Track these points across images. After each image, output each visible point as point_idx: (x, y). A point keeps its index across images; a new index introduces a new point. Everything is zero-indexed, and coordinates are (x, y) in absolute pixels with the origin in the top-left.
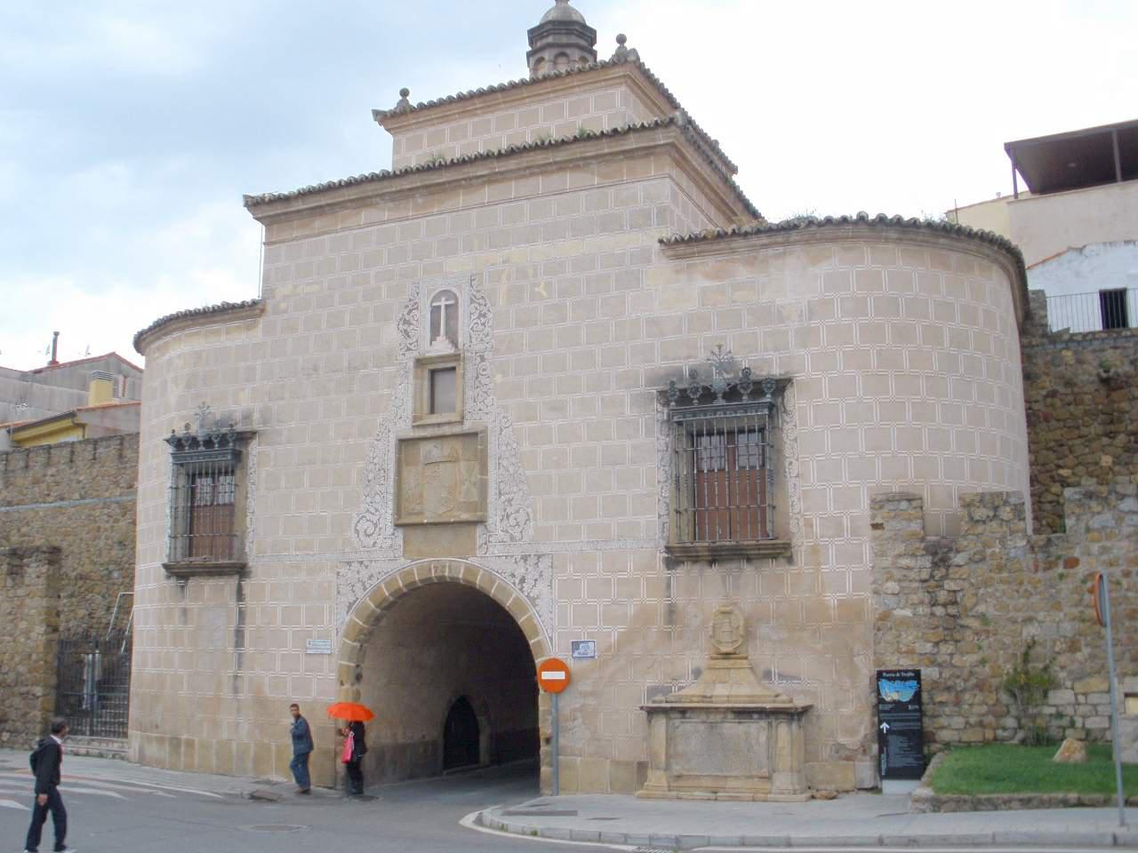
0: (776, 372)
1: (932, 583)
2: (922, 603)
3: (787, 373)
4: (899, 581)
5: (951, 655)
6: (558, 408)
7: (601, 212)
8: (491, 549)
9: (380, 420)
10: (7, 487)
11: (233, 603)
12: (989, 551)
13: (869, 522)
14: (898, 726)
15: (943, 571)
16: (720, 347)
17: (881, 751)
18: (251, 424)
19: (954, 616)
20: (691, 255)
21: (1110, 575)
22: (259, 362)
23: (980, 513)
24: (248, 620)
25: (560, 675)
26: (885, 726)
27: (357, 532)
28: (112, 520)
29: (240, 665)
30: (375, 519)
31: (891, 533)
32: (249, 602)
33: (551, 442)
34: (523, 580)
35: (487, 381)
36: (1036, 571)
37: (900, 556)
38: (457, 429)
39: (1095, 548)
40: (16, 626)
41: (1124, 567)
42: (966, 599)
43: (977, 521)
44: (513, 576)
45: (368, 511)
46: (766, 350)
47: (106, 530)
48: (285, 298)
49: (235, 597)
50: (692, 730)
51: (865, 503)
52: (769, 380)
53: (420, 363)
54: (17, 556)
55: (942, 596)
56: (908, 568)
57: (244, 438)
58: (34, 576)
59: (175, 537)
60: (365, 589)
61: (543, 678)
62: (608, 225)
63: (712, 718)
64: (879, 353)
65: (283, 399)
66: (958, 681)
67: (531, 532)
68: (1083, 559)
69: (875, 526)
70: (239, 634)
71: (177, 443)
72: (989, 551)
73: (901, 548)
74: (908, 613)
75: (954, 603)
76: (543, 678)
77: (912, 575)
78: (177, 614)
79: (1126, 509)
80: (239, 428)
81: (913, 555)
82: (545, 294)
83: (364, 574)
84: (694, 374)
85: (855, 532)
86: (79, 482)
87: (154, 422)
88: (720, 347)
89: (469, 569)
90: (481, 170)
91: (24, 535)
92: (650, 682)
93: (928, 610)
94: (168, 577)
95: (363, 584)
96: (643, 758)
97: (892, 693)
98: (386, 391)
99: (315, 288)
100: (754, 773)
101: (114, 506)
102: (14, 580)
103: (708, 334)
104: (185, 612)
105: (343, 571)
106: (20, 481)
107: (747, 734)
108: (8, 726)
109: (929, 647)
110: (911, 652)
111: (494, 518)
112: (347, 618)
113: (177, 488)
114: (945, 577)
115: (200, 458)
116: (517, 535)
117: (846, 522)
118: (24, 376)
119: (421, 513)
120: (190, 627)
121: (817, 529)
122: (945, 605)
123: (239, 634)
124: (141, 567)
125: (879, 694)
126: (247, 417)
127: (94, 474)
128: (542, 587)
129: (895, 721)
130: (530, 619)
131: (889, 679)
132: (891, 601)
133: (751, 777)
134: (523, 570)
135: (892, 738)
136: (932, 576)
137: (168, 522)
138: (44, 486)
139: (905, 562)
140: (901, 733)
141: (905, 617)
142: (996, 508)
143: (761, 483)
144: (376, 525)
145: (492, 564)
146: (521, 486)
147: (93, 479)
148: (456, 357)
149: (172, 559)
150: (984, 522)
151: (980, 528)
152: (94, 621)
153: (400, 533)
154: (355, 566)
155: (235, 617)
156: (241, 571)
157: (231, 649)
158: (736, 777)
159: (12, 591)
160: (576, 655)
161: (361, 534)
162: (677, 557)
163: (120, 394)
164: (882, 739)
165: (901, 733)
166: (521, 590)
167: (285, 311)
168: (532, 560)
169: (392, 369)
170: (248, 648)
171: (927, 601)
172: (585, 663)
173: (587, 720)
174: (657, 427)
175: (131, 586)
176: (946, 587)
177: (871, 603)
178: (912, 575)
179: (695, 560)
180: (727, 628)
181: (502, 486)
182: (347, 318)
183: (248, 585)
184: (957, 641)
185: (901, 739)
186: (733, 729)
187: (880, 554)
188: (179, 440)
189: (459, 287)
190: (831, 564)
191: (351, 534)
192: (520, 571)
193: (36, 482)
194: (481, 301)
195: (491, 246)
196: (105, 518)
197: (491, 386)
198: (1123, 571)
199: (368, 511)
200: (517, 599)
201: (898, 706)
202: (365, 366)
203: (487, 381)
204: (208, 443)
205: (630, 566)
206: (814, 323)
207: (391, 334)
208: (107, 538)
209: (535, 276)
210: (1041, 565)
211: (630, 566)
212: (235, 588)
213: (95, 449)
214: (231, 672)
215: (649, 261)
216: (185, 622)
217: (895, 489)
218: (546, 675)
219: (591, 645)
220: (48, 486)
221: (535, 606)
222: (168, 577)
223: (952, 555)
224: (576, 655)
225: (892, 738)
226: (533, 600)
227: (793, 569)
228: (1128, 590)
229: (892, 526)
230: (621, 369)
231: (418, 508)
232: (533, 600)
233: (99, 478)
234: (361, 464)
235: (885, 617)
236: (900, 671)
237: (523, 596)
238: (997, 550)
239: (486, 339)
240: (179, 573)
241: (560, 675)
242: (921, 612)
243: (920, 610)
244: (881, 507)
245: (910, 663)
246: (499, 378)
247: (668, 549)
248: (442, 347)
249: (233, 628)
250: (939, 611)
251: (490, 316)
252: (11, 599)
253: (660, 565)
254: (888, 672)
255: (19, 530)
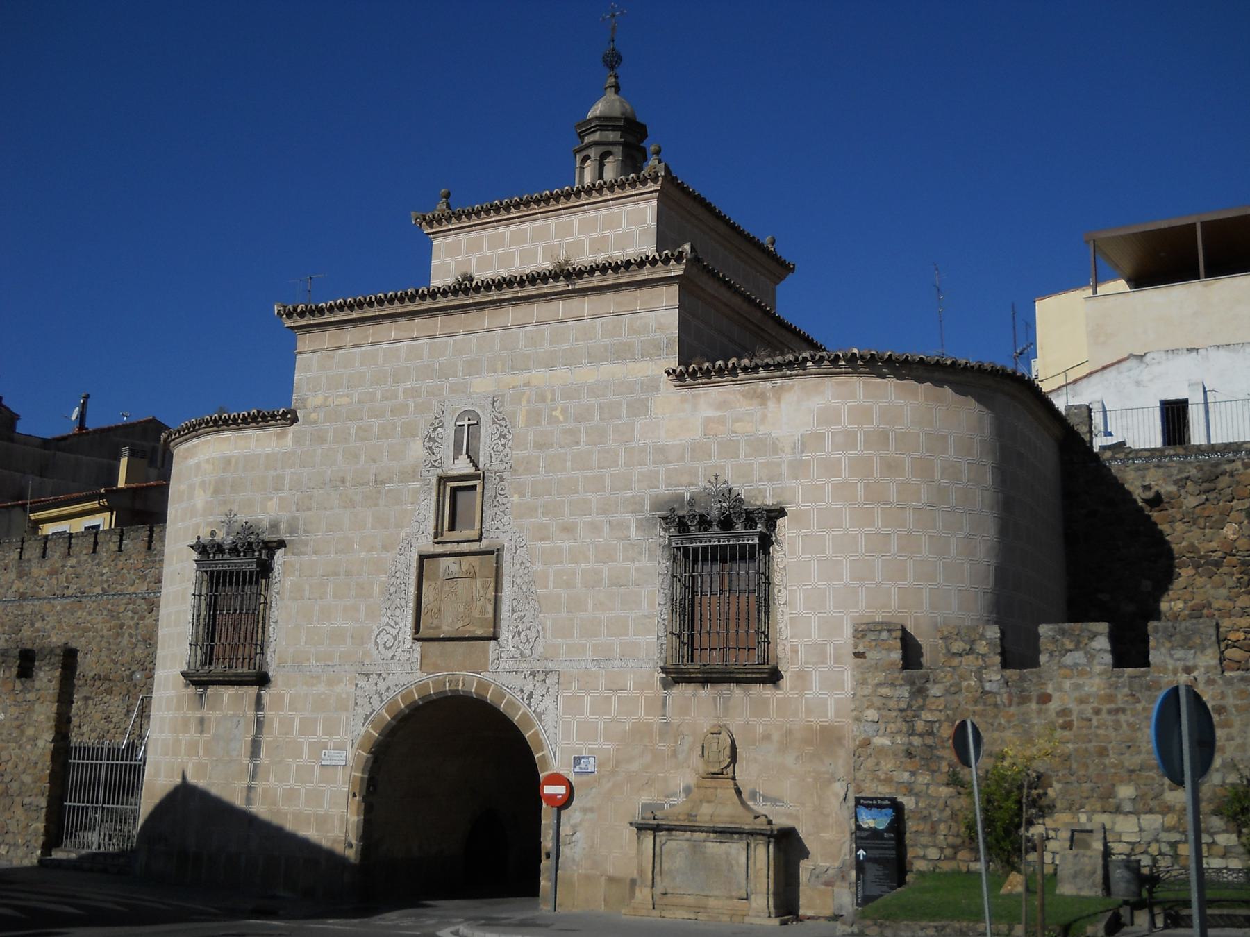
0: (770, 501)
1: (909, 713)
2: (899, 732)
3: (779, 503)
4: (879, 709)
5: (928, 785)
6: (568, 529)
7: (616, 340)
8: (502, 665)
9: (403, 534)
10: (21, 577)
11: (251, 714)
12: (965, 684)
13: (851, 650)
14: (876, 853)
15: (920, 701)
16: (716, 477)
17: (858, 878)
18: (278, 532)
19: (930, 746)
21: (1081, 712)
22: (288, 471)
23: (958, 646)
24: (265, 730)
26: (861, 852)
27: (377, 644)
28: (136, 617)
29: (254, 777)
30: (394, 632)
31: (873, 662)
32: (268, 713)
33: (561, 562)
34: (531, 696)
35: (505, 501)
36: (1010, 705)
37: (880, 685)
38: (475, 547)
39: (1067, 684)
40: (23, 733)
41: (1095, 705)
42: (942, 731)
43: (955, 654)
44: (522, 691)
45: (388, 624)
46: (761, 480)
47: (129, 627)
48: (316, 408)
49: (253, 707)
50: (676, 845)
51: (848, 632)
52: (760, 510)
53: (442, 480)
54: (26, 663)
55: (920, 726)
56: (887, 697)
57: (272, 547)
58: (45, 680)
59: (196, 645)
60: (382, 701)
61: (545, 792)
62: (623, 353)
63: (697, 835)
64: (867, 486)
65: (309, 509)
66: (933, 811)
67: (541, 649)
68: (1056, 695)
69: (858, 655)
71: (202, 549)
72: (965, 684)
73: (880, 677)
74: (886, 741)
75: (931, 733)
76: (545, 792)
77: (892, 704)
78: (193, 723)
79: (1098, 647)
80: (266, 537)
81: (893, 685)
82: (561, 418)
83: (382, 686)
84: (692, 502)
85: (837, 659)
86: (102, 575)
88: (716, 477)
89: (480, 684)
90: (506, 294)
91: (38, 630)
92: (645, 799)
93: (906, 740)
94: (187, 686)
95: (381, 696)
96: (635, 875)
97: (870, 820)
98: (410, 507)
99: (345, 400)
100: (734, 894)
101: (139, 601)
102: (23, 684)
103: (710, 463)
104: (202, 721)
105: (361, 683)
106: (35, 571)
107: (728, 854)
108: (8, 838)
109: (906, 776)
110: (888, 781)
111: (505, 633)
112: (363, 730)
113: (200, 595)
114: (922, 708)
115: (223, 563)
116: (527, 652)
117: (830, 650)
118: (46, 443)
119: (438, 627)
120: (207, 736)
121: (802, 654)
122: (921, 735)
124: (159, 674)
125: (857, 820)
126: (274, 526)
127: (119, 567)
128: (548, 701)
129: (871, 848)
130: (536, 734)
131: (867, 806)
132: (871, 729)
133: (731, 898)
134: (531, 686)
135: (868, 866)
136: (910, 706)
137: (188, 630)
138: (62, 578)
139: (884, 691)
140: (875, 861)
141: (883, 746)
142: (973, 642)
143: (255, 625)
144: (395, 638)
145: (502, 677)
146: (532, 603)
147: (118, 572)
148: (475, 477)
149: (192, 667)
150: (961, 655)
151: (956, 662)
152: (112, 726)
153: (418, 645)
154: (373, 678)
156: (262, 680)
157: (246, 760)
158: (716, 897)
159: (21, 695)
160: (577, 769)
162: (675, 676)
163: (159, 464)
164: (860, 866)
165: (875, 861)
166: (529, 705)
167: (315, 422)
168: (540, 677)
169: (416, 485)
170: (264, 759)
171: (904, 730)
172: (585, 778)
173: (589, 844)
174: (659, 551)
175: (150, 690)
176: (923, 717)
177: (853, 733)
178: (892, 704)
179: (689, 680)
180: (715, 747)
181: (515, 603)
182: (376, 431)
183: (267, 694)
184: (933, 772)
185: (877, 866)
186: (715, 848)
188: (204, 546)
189: (482, 407)
190: (815, 690)
191: (371, 646)
192: (528, 687)
193: (54, 573)
194: (502, 422)
195: (513, 369)
196: (130, 614)
197: (509, 505)
198: (1093, 708)
199: (388, 624)
200: (525, 714)
201: (874, 833)
203: (505, 501)
204: (234, 550)
205: (630, 684)
207: (417, 450)
208: (131, 635)
209: (553, 400)
210: (1015, 700)
211: (630, 684)
212: (254, 697)
213: (121, 541)
214: (244, 783)
215: (657, 389)
216: (202, 732)
217: (879, 618)
218: (548, 790)
219: (592, 760)
220: (67, 578)
221: (541, 721)
222: (187, 686)
223: (928, 686)
224: (577, 769)
225: (868, 866)
226: (539, 715)
227: (779, 694)
228: (1098, 727)
229: (873, 655)
230: (630, 494)
231: (436, 622)
232: (539, 715)
233: (125, 571)
234: (383, 578)
235: (867, 743)
236: (876, 799)
237: (530, 712)
238: (973, 683)
239: (506, 460)
240: (198, 680)
241: (561, 790)
242: (899, 741)
243: (898, 740)
244: (864, 636)
245: (888, 790)
246: (516, 498)
247: (664, 669)
248: (463, 466)
249: (249, 738)
250: (916, 741)
251: (510, 437)
252: (17, 704)
253: (657, 683)
254: (865, 799)
255: (32, 625)
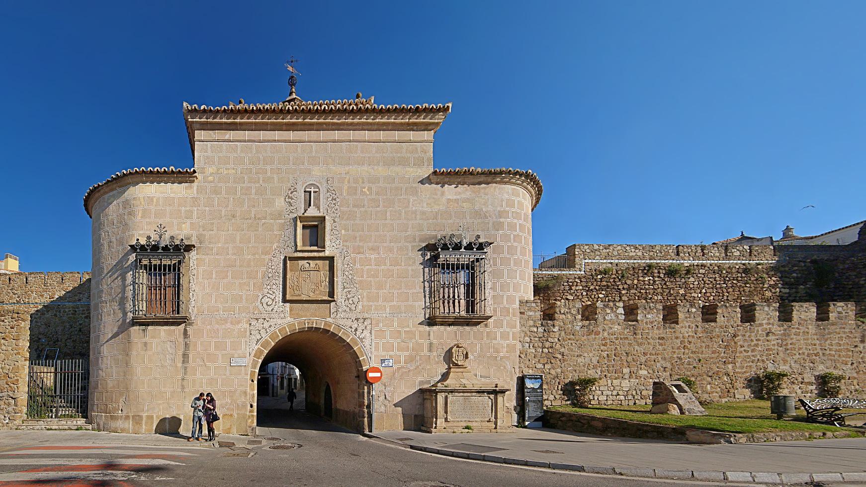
11: (181, 339)
14: (533, 399)
20: (480, 183)
25: (378, 375)
30: (273, 297)
34: (356, 330)
55: (547, 344)
70: (185, 356)
75: (551, 347)
83: (266, 325)
87: (357, 222)
123: (185, 356)
128: (366, 333)
145: (339, 320)
154: (261, 321)
155: (182, 347)
161: (265, 305)
187: (522, 325)
189: (320, 183)
192: (355, 326)
202: (265, 218)
206: (502, 220)
207: (280, 203)
226: (361, 339)
241: (378, 375)
